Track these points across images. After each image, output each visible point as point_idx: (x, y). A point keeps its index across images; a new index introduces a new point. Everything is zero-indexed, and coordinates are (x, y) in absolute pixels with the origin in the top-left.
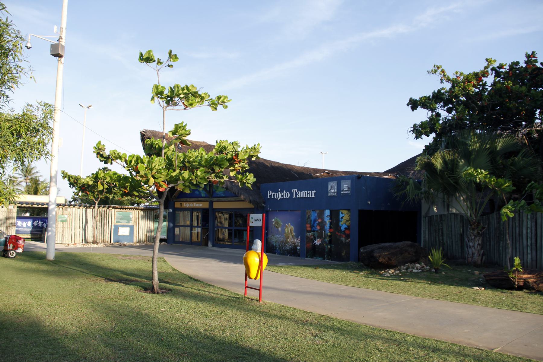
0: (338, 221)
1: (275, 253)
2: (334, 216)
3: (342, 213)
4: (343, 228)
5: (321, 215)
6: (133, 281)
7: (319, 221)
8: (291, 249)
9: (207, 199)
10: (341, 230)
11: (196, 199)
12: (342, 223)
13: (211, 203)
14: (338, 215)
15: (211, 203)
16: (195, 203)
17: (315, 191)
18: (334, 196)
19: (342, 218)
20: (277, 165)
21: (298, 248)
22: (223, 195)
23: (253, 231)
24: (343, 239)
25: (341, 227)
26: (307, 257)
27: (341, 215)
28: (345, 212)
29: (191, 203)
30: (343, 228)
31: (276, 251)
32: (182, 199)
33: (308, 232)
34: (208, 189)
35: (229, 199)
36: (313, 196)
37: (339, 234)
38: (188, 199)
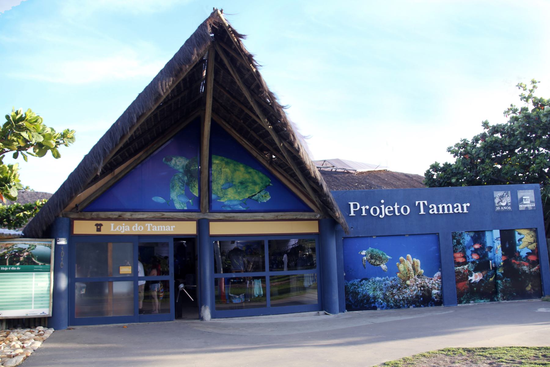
0: (513, 245)
1: (375, 308)
2: (508, 239)
3: (519, 234)
4: (523, 254)
5: (216, 242)
6: (153, 361)
7: (477, 246)
8: (417, 296)
9: (195, 215)
10: (520, 257)
11: (158, 215)
12: (521, 247)
13: (203, 225)
14: (513, 237)
15: (203, 225)
16: (149, 224)
17: (468, 205)
18: (506, 211)
19: (520, 240)
20: (169, 83)
21: (434, 292)
22: (241, 208)
23: (240, 282)
24: (525, 268)
25: (519, 253)
26: (460, 302)
27: (518, 237)
28: (524, 232)
29: (136, 224)
30: (523, 254)
31: (377, 304)
32: (102, 214)
33: (459, 264)
34: (196, 194)
35: (259, 215)
36: (465, 211)
37: (518, 262)
38: (128, 215)
